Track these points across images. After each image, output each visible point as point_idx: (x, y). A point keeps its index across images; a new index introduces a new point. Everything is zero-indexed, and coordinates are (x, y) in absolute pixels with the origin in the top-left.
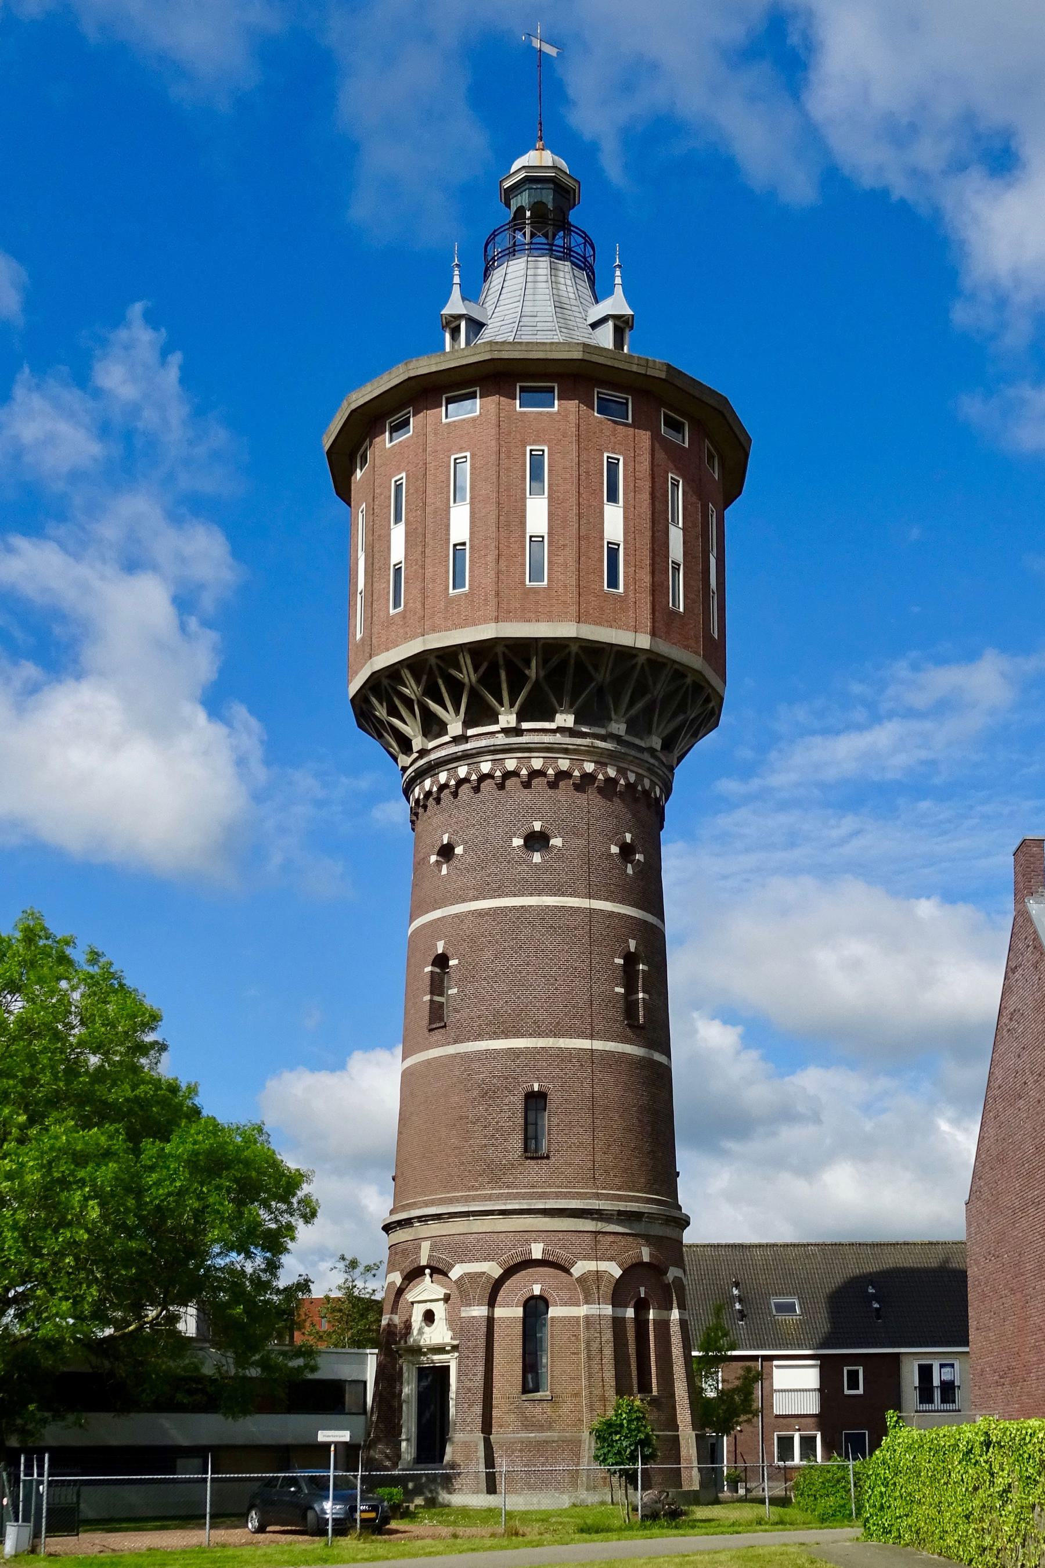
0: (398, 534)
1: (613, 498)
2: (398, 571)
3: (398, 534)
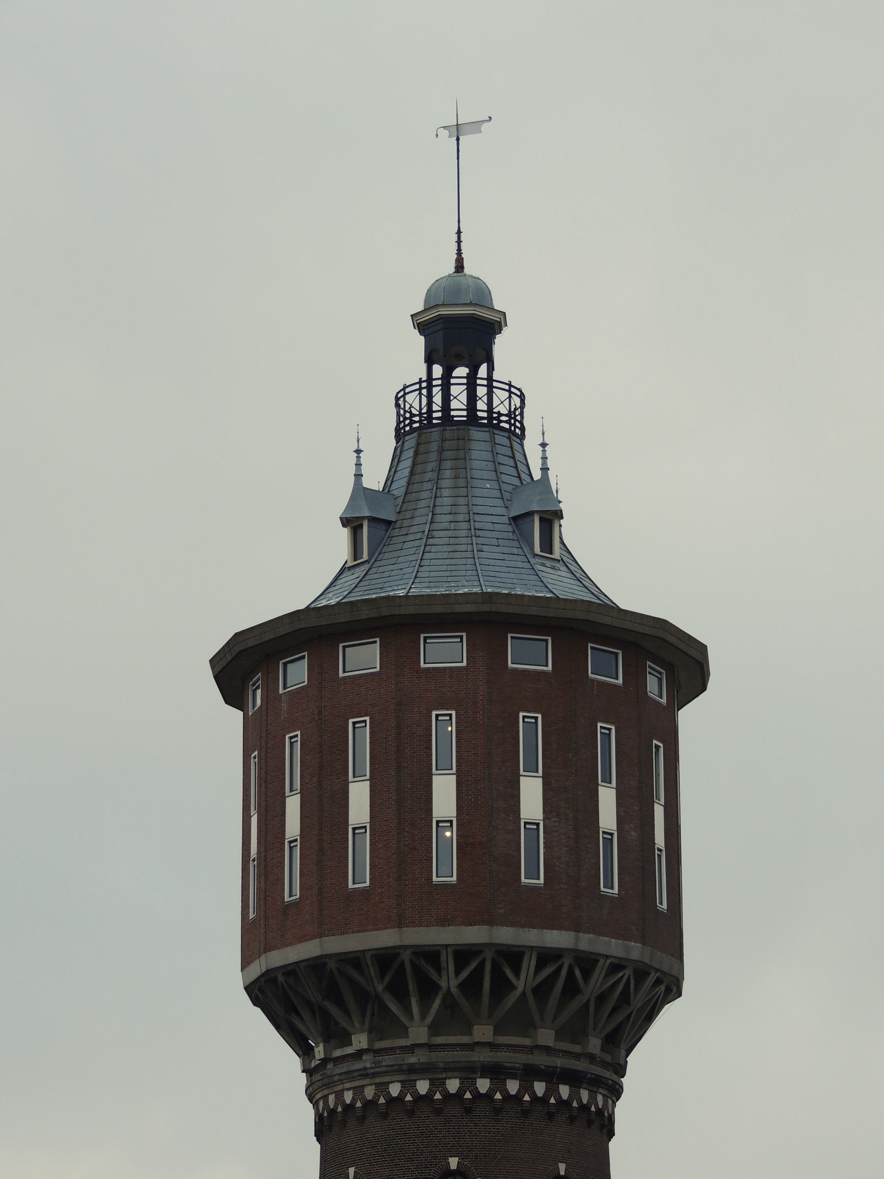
0: (608, 816)
3: (608, 816)
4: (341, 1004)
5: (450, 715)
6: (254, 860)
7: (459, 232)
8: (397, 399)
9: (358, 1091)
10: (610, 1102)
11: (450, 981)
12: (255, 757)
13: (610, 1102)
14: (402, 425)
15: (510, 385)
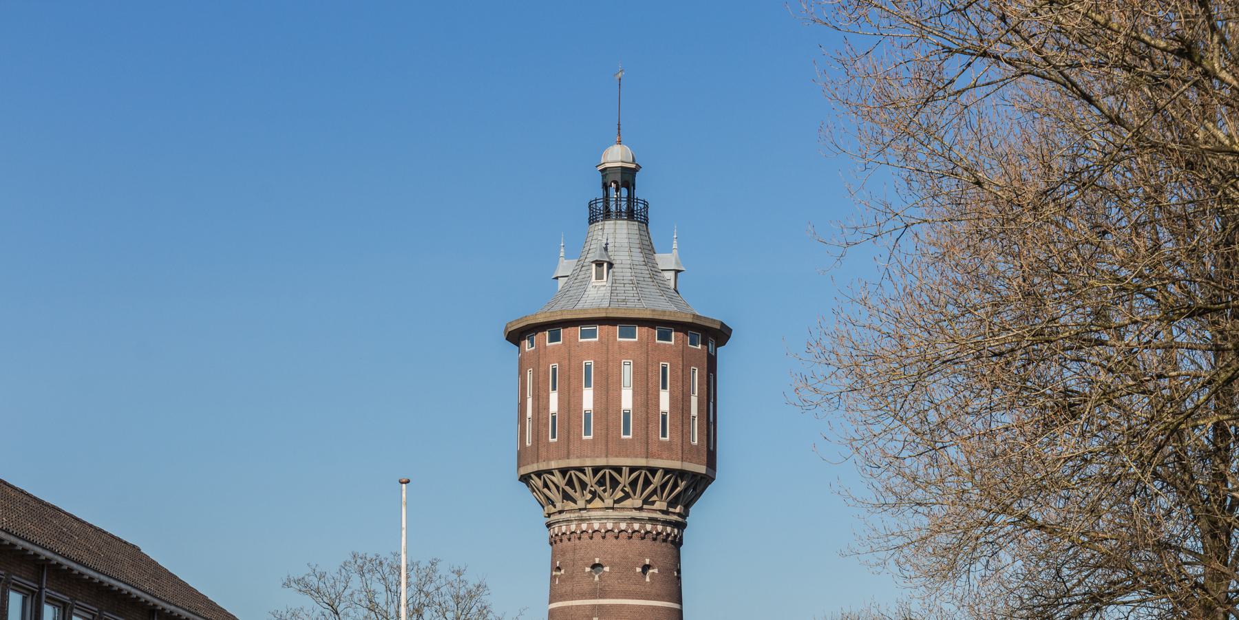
0: (554, 397)
1: (664, 387)
2: (554, 418)
3: (554, 397)
4: (573, 487)
9: (578, 526)
11: (624, 480)
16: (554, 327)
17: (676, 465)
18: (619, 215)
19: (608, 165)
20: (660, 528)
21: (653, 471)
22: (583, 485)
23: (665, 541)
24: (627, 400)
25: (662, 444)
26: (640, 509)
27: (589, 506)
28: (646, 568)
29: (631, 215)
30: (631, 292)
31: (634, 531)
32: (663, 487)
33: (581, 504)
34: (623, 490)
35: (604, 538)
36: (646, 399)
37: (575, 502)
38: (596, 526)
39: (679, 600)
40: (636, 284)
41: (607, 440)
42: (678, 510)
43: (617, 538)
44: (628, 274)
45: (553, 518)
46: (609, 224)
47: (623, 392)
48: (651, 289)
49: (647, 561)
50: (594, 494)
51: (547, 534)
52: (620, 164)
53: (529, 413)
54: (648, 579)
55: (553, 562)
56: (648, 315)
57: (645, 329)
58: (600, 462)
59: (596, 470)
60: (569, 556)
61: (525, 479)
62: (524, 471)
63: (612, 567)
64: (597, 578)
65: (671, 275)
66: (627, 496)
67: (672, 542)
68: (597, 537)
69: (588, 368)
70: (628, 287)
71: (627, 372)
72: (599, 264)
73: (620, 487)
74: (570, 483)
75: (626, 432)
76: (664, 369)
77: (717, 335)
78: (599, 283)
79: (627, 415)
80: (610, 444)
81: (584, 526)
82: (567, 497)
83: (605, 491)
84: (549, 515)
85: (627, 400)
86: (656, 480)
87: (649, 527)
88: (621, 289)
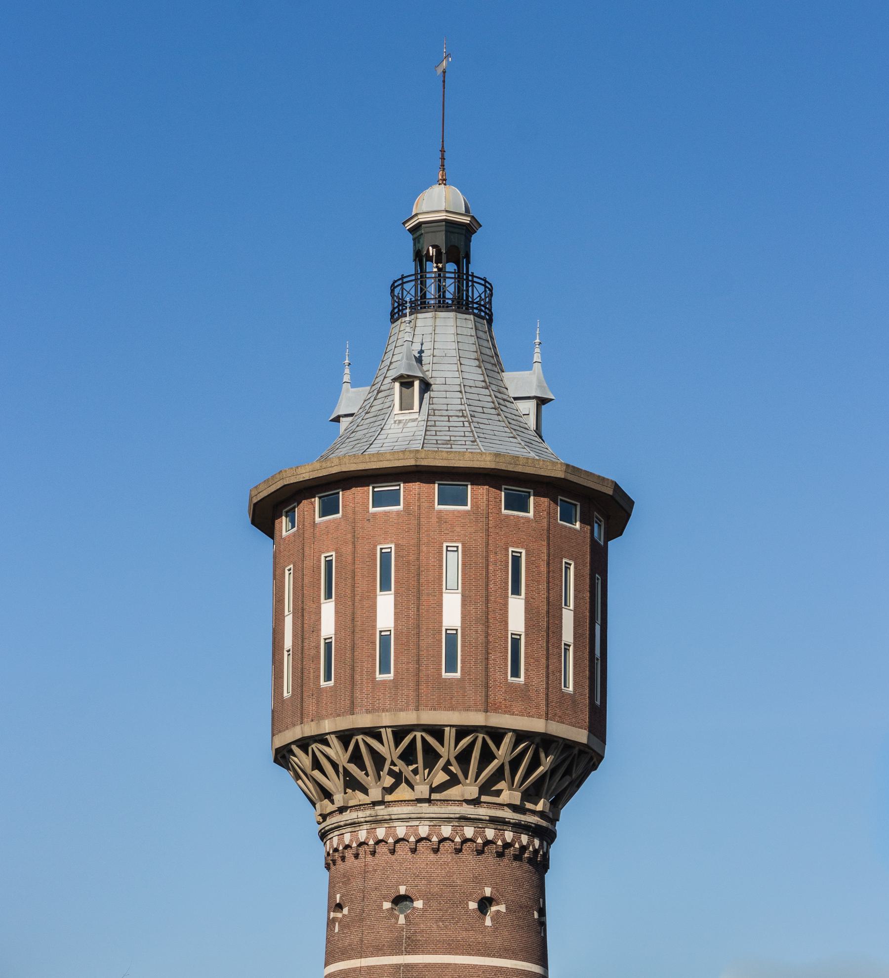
0: (328, 610)
1: (516, 591)
2: (328, 646)
3: (328, 610)
4: (362, 767)
5: (457, 547)
6: (288, 651)
7: (443, 151)
8: (393, 288)
9: (370, 831)
10: (545, 843)
11: (447, 751)
12: (289, 570)
13: (545, 843)
14: (396, 310)
15: (486, 281)
16: (328, 488)
17: (537, 725)
18: (442, 305)
19: (422, 218)
20: (509, 836)
21: (497, 735)
22: (379, 760)
23: (518, 857)
24: (452, 614)
25: (513, 688)
26: (476, 802)
27: (388, 798)
28: (485, 904)
29: (461, 304)
30: (460, 431)
31: (465, 841)
32: (515, 764)
33: (375, 794)
34: (445, 769)
35: (414, 851)
36: (485, 611)
37: (365, 791)
38: (401, 832)
39: (543, 961)
40: (470, 418)
41: (419, 683)
42: (540, 807)
43: (436, 851)
44: (455, 400)
45: (331, 821)
46: (425, 319)
47: (446, 598)
48: (495, 427)
49: (488, 892)
50: (399, 778)
51: (320, 850)
52: (442, 216)
53: (288, 643)
54: (488, 922)
55: (331, 897)
56: (487, 463)
57: (483, 490)
58: (407, 718)
59: (400, 733)
60: (357, 883)
61: (282, 756)
62: (281, 740)
63: (427, 901)
64: (402, 920)
65: (529, 407)
66: (454, 781)
67: (531, 861)
68: (403, 850)
69: (385, 557)
70: (456, 422)
71: (453, 564)
72: (406, 382)
73: (441, 763)
74: (356, 758)
75: (451, 667)
76: (516, 560)
77: (604, 509)
78: (406, 416)
79: (451, 639)
80: (423, 687)
81: (381, 833)
82: (352, 784)
83: (415, 772)
84: (324, 817)
85: (452, 614)
86: (503, 752)
87: (490, 833)
88: (443, 424)
